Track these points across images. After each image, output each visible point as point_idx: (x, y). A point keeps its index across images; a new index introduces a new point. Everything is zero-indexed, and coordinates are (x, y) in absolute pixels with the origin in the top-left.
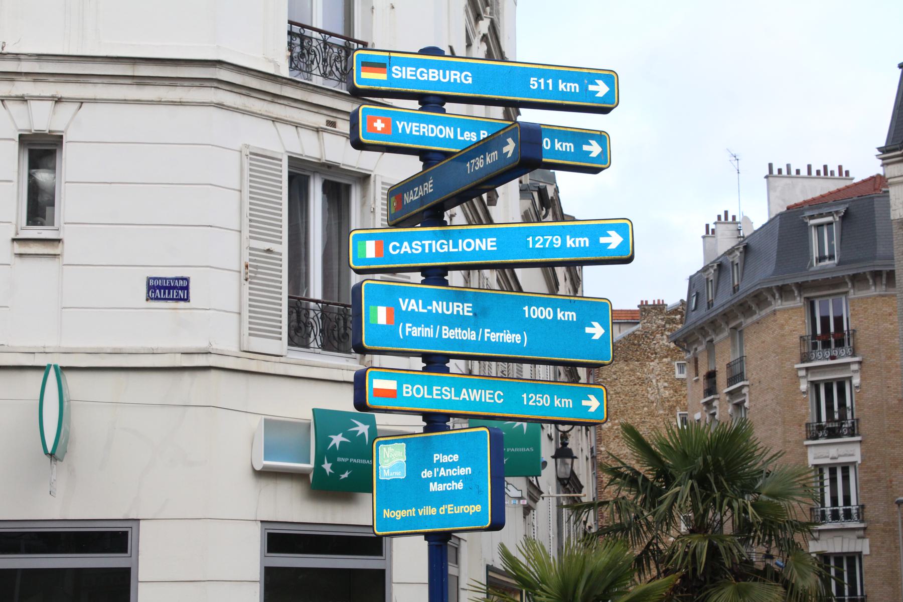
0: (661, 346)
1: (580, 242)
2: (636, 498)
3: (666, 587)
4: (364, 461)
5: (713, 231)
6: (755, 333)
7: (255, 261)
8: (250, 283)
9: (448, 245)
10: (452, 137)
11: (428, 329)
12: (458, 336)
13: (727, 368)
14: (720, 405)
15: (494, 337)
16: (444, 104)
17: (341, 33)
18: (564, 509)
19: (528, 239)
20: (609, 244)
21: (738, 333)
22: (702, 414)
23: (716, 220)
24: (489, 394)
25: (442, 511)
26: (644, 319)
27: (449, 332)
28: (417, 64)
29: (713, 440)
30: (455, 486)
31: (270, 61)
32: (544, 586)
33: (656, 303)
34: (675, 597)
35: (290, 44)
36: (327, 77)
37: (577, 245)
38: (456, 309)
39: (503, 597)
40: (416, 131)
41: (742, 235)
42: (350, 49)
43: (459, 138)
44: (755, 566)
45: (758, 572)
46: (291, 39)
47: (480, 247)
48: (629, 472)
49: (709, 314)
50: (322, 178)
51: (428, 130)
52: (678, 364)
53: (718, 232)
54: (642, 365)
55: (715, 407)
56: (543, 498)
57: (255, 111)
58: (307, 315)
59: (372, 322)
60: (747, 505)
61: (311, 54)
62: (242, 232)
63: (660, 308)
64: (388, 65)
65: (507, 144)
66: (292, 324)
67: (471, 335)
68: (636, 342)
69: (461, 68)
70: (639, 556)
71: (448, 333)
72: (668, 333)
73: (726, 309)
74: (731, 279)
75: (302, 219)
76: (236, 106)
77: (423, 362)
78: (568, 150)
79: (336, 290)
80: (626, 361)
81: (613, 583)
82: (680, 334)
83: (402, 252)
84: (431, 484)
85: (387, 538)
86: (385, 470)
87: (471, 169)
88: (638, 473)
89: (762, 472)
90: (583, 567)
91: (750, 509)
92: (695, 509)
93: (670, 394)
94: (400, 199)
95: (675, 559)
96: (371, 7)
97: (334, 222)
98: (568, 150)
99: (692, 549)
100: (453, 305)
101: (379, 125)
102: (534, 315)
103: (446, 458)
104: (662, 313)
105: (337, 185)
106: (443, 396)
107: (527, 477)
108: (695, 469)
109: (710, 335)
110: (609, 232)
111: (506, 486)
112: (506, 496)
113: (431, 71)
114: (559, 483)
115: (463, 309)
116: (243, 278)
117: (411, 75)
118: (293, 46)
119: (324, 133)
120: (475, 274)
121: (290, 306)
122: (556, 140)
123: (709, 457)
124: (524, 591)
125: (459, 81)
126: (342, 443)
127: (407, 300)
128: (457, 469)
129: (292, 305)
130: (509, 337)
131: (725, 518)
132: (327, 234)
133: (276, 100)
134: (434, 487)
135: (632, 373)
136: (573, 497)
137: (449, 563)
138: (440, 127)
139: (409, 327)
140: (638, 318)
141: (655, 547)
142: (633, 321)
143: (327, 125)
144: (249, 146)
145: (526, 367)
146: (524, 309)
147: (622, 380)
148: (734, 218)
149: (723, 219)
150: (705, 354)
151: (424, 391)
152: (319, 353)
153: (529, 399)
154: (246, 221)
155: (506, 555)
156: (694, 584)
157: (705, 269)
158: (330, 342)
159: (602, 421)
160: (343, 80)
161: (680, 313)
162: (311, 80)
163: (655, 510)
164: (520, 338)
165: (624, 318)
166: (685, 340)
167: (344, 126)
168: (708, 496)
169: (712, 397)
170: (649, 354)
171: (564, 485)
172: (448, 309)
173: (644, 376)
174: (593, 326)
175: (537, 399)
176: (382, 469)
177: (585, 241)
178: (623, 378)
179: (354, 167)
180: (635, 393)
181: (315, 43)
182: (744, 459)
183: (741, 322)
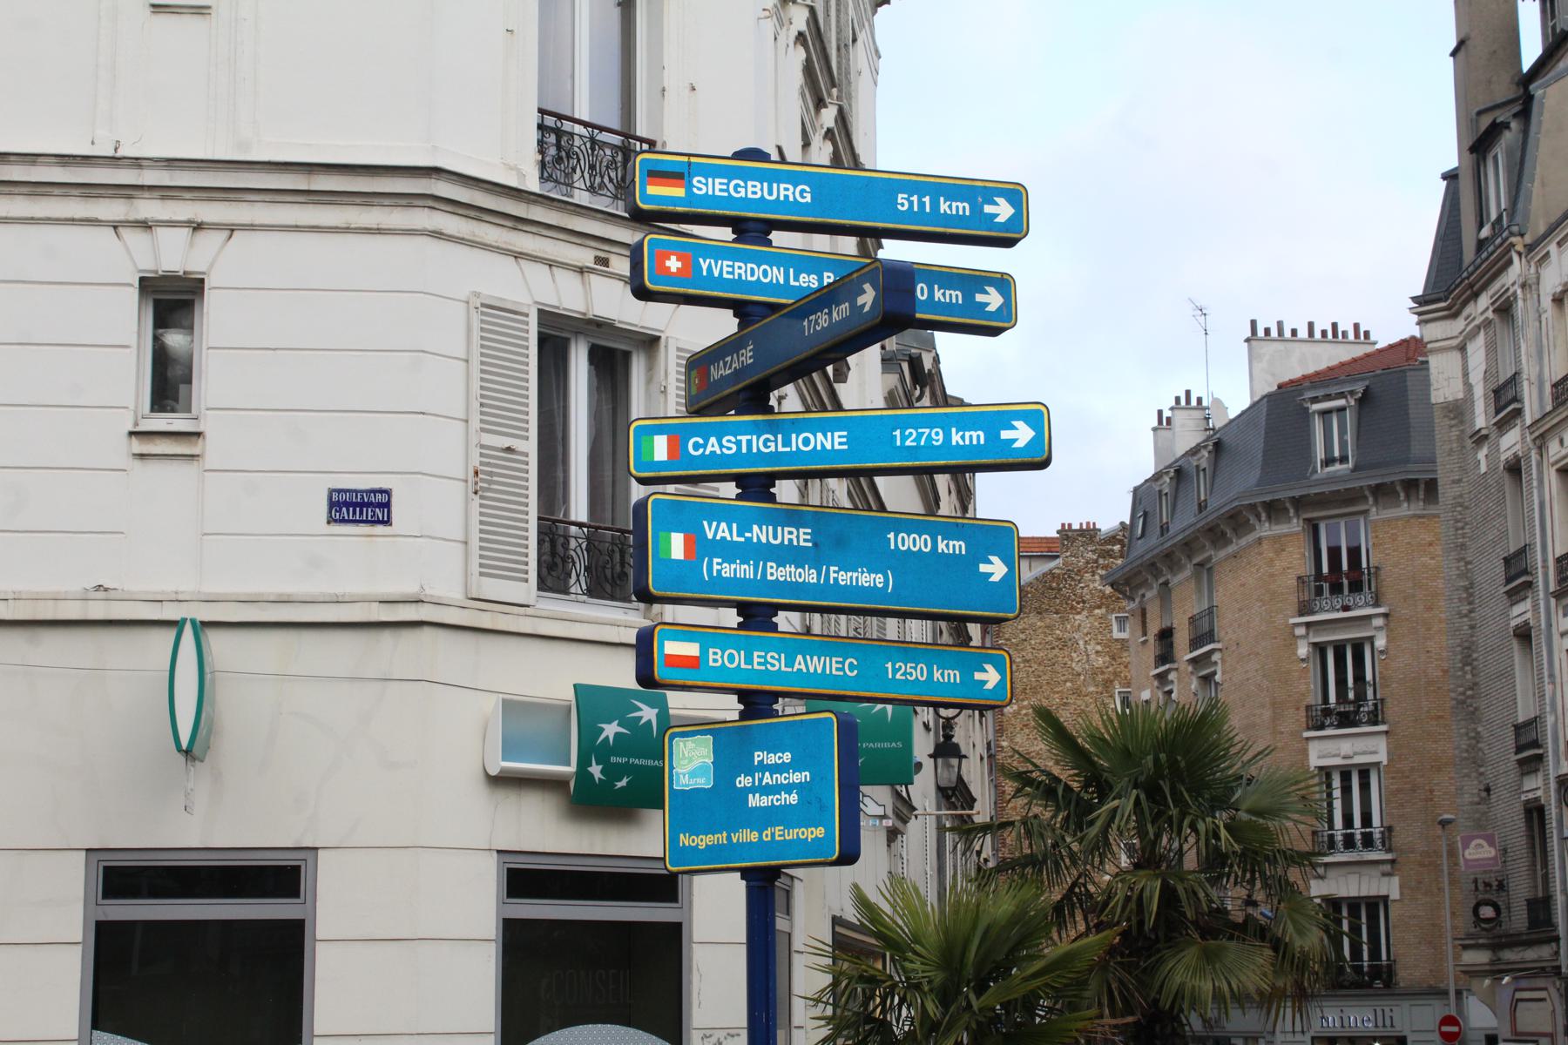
1: (971, 437)
2: (1055, 816)
3: (1099, 949)
4: (650, 763)
5: (1169, 420)
7: (488, 464)
8: (482, 497)
9: (776, 441)
10: (782, 282)
11: (746, 566)
12: (790, 576)
13: (1190, 623)
15: (844, 578)
16: (769, 233)
17: (616, 126)
18: (947, 833)
20: (1015, 440)
21: (1205, 571)
22: (1152, 691)
23: (1173, 403)
24: (836, 662)
25: (767, 836)
27: (777, 570)
30: (785, 798)
31: (511, 169)
32: (918, 948)
33: (1084, 527)
34: (1112, 964)
35: (541, 143)
37: (967, 442)
38: (787, 537)
39: (857, 964)
40: (728, 273)
41: (1211, 426)
43: (792, 283)
44: (1230, 917)
45: (1235, 926)
46: (543, 136)
47: (822, 444)
48: (1044, 778)
50: (589, 342)
51: (746, 272)
52: (1116, 617)
53: (1177, 422)
54: (1064, 620)
56: (916, 817)
57: (488, 242)
58: (566, 545)
59: (662, 556)
60: (1218, 827)
61: (572, 158)
62: (470, 422)
64: (686, 175)
67: (809, 576)
69: (794, 179)
71: (776, 572)
72: (1104, 572)
73: (1189, 535)
76: (461, 236)
78: (954, 301)
79: (609, 507)
81: (1019, 944)
83: (707, 452)
84: (751, 796)
86: (681, 776)
88: (1057, 780)
89: (1241, 777)
91: (1223, 833)
92: (1142, 833)
94: (705, 374)
95: (1113, 908)
96: (660, 89)
97: (606, 408)
98: (954, 301)
99: (1136, 892)
100: (783, 530)
101: (673, 264)
103: (773, 758)
104: (1093, 541)
106: (768, 666)
107: (892, 785)
109: (1164, 575)
111: (861, 799)
112: (861, 813)
113: (750, 183)
114: (940, 795)
115: (798, 537)
116: (471, 489)
117: (721, 190)
119: (591, 275)
122: (936, 286)
123: (1163, 756)
124: (888, 954)
125: (791, 199)
127: (715, 524)
128: (789, 774)
129: (542, 322)
130: (866, 579)
131: (1186, 847)
134: (754, 801)
136: (961, 815)
137: (777, 914)
139: (718, 564)
140: (1059, 549)
143: (595, 263)
145: (892, 623)
146: (888, 536)
147: (1033, 642)
148: (1199, 400)
149: (1183, 402)
150: (1157, 602)
151: (740, 659)
152: (584, 602)
153: (895, 671)
154: (476, 405)
155: (862, 902)
157: (1157, 477)
161: (1120, 542)
162: (572, 196)
163: (1083, 833)
164: (882, 580)
165: (1037, 550)
166: (1127, 582)
167: (622, 265)
168: (1160, 814)
169: (1167, 666)
171: (948, 798)
172: (775, 537)
175: (908, 671)
176: (678, 774)
177: (978, 437)
178: (1036, 639)
179: (636, 326)
181: (577, 142)
183: (1211, 556)
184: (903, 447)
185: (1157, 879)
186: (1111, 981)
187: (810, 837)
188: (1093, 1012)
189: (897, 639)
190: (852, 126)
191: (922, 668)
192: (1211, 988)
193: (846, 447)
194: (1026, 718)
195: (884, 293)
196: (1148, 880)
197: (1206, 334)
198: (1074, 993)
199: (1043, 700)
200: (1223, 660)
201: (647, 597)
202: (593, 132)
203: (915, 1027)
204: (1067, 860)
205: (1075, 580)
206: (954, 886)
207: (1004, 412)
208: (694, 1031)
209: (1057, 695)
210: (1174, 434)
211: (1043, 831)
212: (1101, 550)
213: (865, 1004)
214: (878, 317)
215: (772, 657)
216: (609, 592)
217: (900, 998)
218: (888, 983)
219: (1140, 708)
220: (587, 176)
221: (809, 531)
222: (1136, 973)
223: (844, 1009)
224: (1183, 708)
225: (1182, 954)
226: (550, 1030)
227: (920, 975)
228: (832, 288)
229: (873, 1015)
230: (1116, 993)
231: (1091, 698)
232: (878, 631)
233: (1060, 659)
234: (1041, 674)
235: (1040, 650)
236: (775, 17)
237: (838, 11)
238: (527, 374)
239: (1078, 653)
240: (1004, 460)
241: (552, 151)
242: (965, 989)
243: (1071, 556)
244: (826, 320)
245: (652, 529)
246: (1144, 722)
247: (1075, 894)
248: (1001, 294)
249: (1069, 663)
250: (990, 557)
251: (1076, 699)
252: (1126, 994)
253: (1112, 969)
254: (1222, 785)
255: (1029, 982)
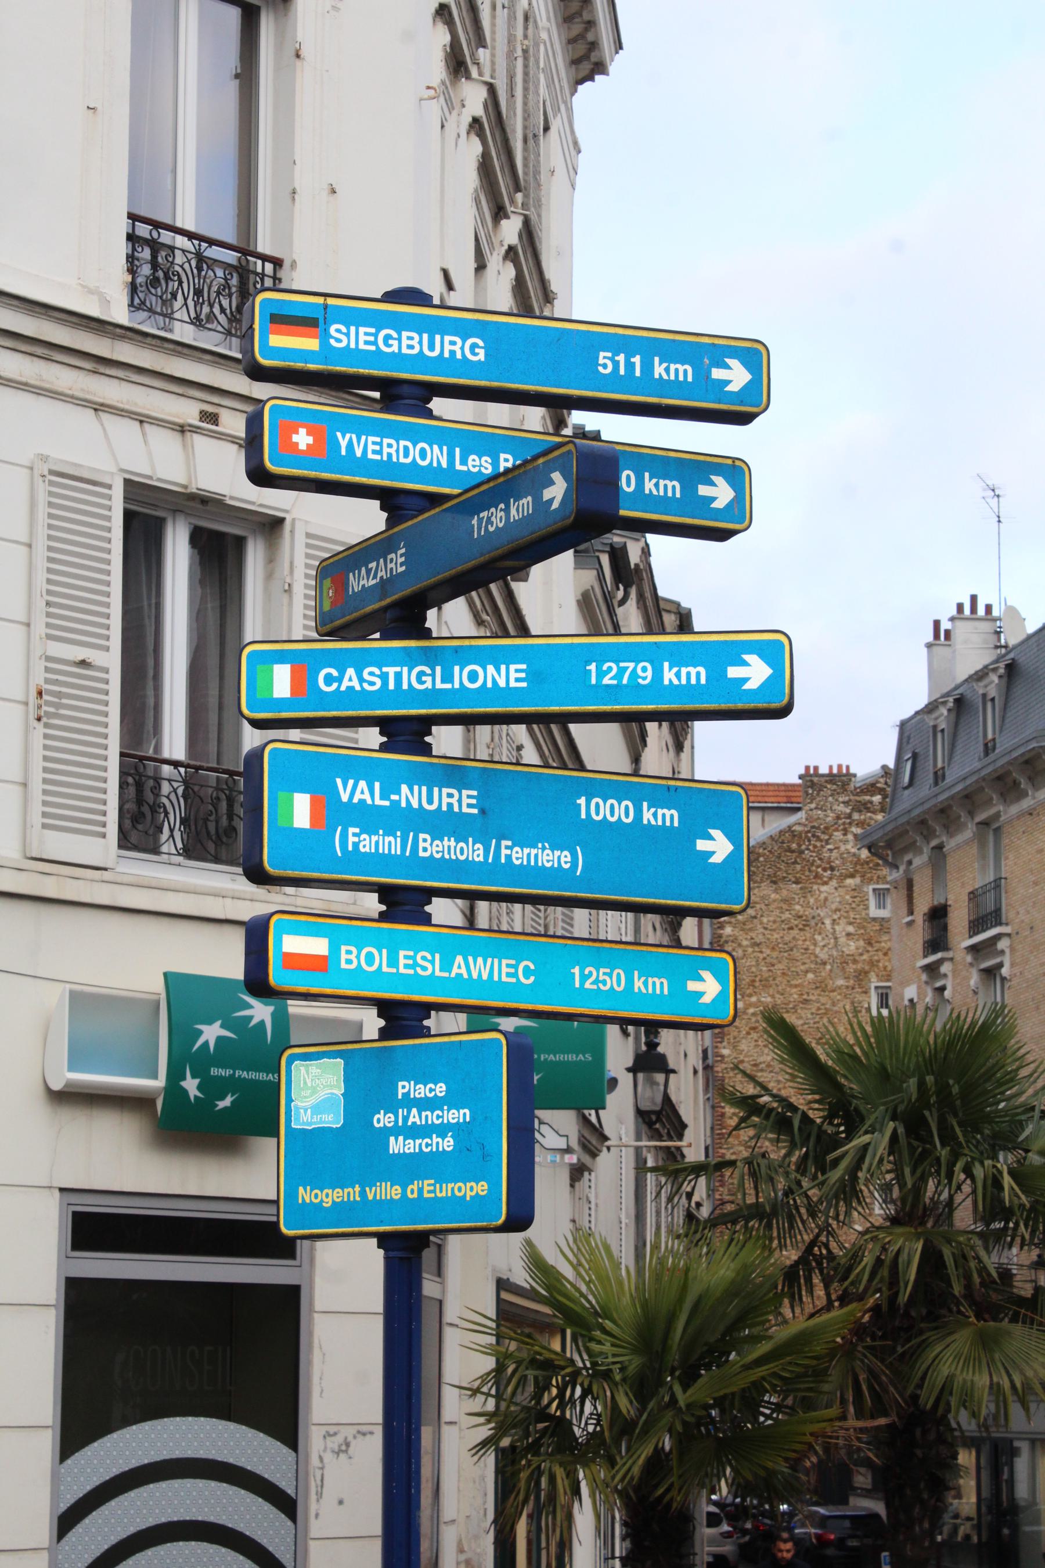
0: (843, 854)
1: (688, 674)
2: (788, 1155)
4: (262, 1076)
6: (1024, 832)
7: (56, 682)
8: (47, 726)
9: (433, 675)
10: (444, 465)
11: (391, 839)
12: (449, 853)
13: (970, 899)
14: (954, 971)
15: (520, 855)
16: (429, 400)
17: (230, 238)
18: (649, 1174)
19: (588, 668)
20: (746, 680)
21: (991, 832)
22: (919, 988)
23: (953, 612)
24: (508, 966)
25: (412, 1192)
26: (811, 802)
27: (431, 845)
28: (378, 321)
29: (939, 1049)
30: (438, 1143)
31: (91, 292)
32: (608, 1324)
33: (835, 771)
34: (860, 1348)
35: (131, 258)
36: (203, 326)
37: (684, 681)
38: (445, 800)
39: (528, 1344)
40: (374, 452)
41: (1003, 642)
42: (249, 271)
43: (459, 467)
44: (1015, 1290)
45: (1021, 1301)
46: (134, 249)
47: (494, 680)
48: (775, 1105)
49: (936, 796)
50: (190, 523)
51: (397, 451)
52: (874, 890)
54: (806, 892)
55: (945, 975)
56: (609, 1148)
57: (60, 389)
58: (156, 790)
60: (1001, 1173)
62: (32, 626)
63: (842, 781)
64: (321, 321)
65: (552, 483)
66: (127, 806)
67: (475, 852)
68: (794, 846)
69: (463, 330)
70: (791, 1266)
71: (430, 847)
72: (858, 831)
73: (970, 785)
74: (981, 728)
75: (149, 598)
76: (24, 380)
77: (381, 901)
78: (670, 494)
79: (213, 735)
80: (775, 882)
81: (741, 1320)
82: (880, 833)
83: (343, 688)
84: (392, 1139)
85: (304, 1241)
86: (302, 1111)
87: (479, 529)
88: (794, 1108)
89: (1033, 1108)
90: (684, 1289)
91: (1007, 1180)
93: (857, 949)
94: (341, 585)
95: (858, 1274)
96: (290, 190)
98: (670, 494)
99: (891, 1255)
100: (440, 791)
101: (303, 439)
102: (597, 814)
103: (422, 1091)
104: (846, 790)
105: (219, 537)
106: (419, 970)
107: (579, 1109)
108: (902, 1102)
109: (938, 836)
110: (745, 657)
111: (536, 1126)
112: (537, 1146)
114: (640, 1120)
115: (460, 801)
116: (32, 717)
117: (366, 343)
118: (136, 262)
119: (195, 436)
120: (483, 732)
121: (123, 773)
122: (647, 475)
123: (930, 1079)
124: (569, 1332)
125: (459, 356)
126: (220, 1040)
127: (351, 782)
128: (442, 1111)
129: (126, 770)
130: (548, 857)
131: (958, 1198)
132: (198, 629)
133: (102, 369)
134: (397, 1145)
135: (785, 907)
136: (668, 1148)
137: (425, 1275)
138: (421, 445)
139: (354, 835)
140: (799, 800)
141: (824, 1252)
142: (789, 805)
143: (201, 420)
144: (47, 457)
145: (581, 915)
146: (578, 801)
147: (765, 920)
148: (989, 608)
149: (967, 611)
150: (928, 872)
151: (381, 960)
152: (179, 865)
153: (584, 978)
155: (537, 1263)
156: (897, 1323)
157: (931, 708)
158: (200, 841)
159: (726, 1022)
160: (233, 331)
161: (881, 791)
162: (171, 331)
163: (826, 1176)
164: (569, 859)
165: (773, 799)
166: (889, 845)
167: (235, 424)
168: (925, 1154)
169: (939, 955)
170: (819, 870)
171: (650, 1124)
172: (430, 801)
173: (808, 912)
174: (710, 838)
176: (297, 1108)
177: (698, 674)
178: (768, 916)
179: (253, 503)
180: (791, 945)
181: (179, 259)
182: (1000, 1084)
183: (999, 812)
184: (598, 686)
185: (918, 1239)
186: (858, 1370)
187: (469, 1194)
188: (834, 1411)
189: (587, 936)
190: (540, 243)
191: (619, 974)
192: (988, 1383)
193: (524, 685)
194: (754, 1019)
195: (581, 484)
196: (906, 1240)
197: (999, 521)
198: (812, 1385)
199: (777, 996)
200: (1012, 949)
201: (258, 875)
202: (200, 245)
203: (601, 1426)
204: (803, 1211)
205: (821, 841)
206: (656, 1247)
207: (733, 642)
208: (313, 1428)
209: (794, 990)
210: (954, 651)
211: (773, 1175)
212: (857, 801)
213: (538, 1396)
214: (570, 517)
215: (424, 958)
216: (213, 852)
217: (583, 1390)
218: (569, 1370)
219: (902, 1013)
220: (191, 303)
221: (475, 793)
222: (891, 1359)
223: (511, 1402)
224: (959, 1016)
225: (949, 1339)
226: (127, 1422)
227: (610, 1360)
228: (510, 476)
229: (548, 1411)
230: (864, 1387)
231: (840, 994)
232: (563, 921)
233: (800, 942)
234: (775, 961)
235: (774, 930)
236: (442, 99)
237: (526, 89)
238: (109, 564)
239: (824, 935)
240: (731, 706)
241: (146, 270)
242: (669, 1379)
243: (816, 808)
244: (501, 517)
245: (269, 787)
246: (907, 1034)
247: (814, 1255)
248: (731, 486)
249: (812, 947)
250: (711, 831)
251: (819, 995)
252: (877, 1387)
253: (860, 1356)
254: (1007, 1119)
255: (751, 1372)
